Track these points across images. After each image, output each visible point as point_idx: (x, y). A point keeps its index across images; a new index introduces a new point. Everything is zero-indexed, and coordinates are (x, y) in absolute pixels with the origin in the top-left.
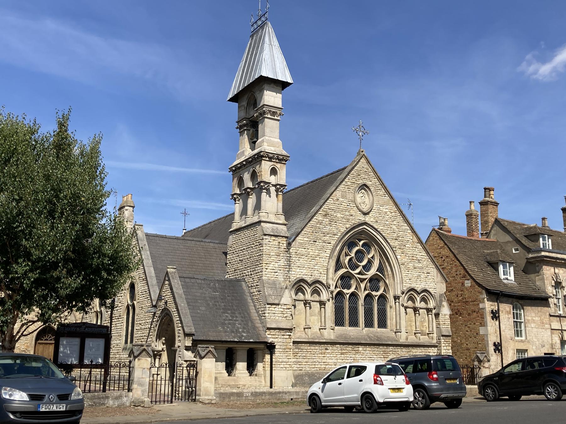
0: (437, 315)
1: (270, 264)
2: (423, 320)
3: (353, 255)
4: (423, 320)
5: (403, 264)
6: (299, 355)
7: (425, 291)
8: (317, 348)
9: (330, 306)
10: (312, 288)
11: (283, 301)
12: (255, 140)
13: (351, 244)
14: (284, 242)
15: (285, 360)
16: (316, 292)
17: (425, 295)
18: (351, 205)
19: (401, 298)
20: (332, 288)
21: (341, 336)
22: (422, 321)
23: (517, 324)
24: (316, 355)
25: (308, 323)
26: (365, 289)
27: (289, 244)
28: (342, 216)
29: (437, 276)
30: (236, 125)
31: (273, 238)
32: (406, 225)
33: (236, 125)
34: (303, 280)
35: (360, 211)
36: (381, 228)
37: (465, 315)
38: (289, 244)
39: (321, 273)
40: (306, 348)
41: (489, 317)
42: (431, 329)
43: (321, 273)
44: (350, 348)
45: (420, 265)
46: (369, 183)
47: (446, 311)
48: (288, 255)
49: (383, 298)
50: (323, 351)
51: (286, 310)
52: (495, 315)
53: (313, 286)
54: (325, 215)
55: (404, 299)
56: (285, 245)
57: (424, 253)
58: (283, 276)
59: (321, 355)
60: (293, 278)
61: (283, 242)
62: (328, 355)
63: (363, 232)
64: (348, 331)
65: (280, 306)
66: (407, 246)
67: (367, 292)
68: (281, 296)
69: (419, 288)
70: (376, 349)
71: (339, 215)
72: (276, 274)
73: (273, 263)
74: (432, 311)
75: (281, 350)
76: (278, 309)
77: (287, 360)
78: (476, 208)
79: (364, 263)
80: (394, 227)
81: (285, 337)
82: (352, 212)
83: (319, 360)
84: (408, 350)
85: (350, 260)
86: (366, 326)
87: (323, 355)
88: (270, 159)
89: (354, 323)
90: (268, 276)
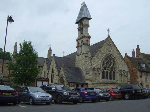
0: (127, 76)
3: (107, 62)
7: (124, 70)
9: (101, 74)
12: (82, 33)
13: (106, 59)
16: (98, 71)
20: (102, 70)
23: (146, 79)
25: (96, 78)
26: (110, 70)
27: (91, 59)
30: (77, 29)
31: (87, 57)
33: (77, 29)
34: (95, 68)
35: (109, 50)
37: (133, 76)
38: (91, 59)
41: (139, 77)
44: (106, 84)
45: (123, 64)
46: (111, 44)
47: (129, 75)
49: (114, 73)
52: (141, 77)
55: (119, 73)
57: (124, 61)
64: (106, 80)
67: (110, 71)
68: (89, 72)
76: (89, 75)
78: (135, 50)
79: (109, 64)
85: (106, 63)
89: (107, 78)
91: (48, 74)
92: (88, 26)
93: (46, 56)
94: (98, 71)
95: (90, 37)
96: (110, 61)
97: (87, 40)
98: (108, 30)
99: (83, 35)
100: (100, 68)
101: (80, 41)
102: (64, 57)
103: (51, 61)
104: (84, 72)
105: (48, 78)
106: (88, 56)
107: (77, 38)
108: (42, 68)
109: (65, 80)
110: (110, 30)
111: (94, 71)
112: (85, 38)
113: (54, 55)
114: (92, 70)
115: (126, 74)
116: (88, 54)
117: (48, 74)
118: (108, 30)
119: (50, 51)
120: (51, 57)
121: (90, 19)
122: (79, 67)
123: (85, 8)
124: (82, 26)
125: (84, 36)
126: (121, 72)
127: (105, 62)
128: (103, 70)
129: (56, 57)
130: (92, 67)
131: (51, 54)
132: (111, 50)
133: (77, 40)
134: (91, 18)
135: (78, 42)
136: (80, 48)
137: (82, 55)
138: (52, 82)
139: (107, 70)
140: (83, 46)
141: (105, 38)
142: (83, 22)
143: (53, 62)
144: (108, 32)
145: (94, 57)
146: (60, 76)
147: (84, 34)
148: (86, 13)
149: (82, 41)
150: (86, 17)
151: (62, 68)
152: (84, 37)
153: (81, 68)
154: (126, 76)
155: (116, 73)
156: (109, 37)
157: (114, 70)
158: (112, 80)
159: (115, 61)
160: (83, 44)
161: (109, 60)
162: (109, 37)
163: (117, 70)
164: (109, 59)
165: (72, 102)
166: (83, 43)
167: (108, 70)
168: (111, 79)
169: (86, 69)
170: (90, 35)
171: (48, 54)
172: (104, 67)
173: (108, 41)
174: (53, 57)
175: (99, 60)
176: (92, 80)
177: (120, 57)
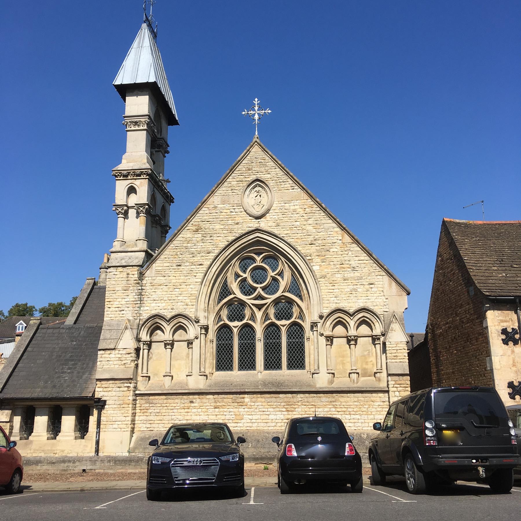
1: (114, 301)
2: (366, 353)
4: (366, 353)
5: (324, 277)
6: (150, 411)
8: (176, 401)
10: (172, 324)
11: (121, 345)
14: (134, 273)
15: (119, 419)
17: (366, 316)
18: (236, 210)
19: (319, 325)
21: (216, 384)
22: (364, 356)
24: (174, 411)
27: (141, 275)
28: (222, 227)
29: (390, 285)
31: (120, 269)
32: (330, 221)
36: (286, 232)
38: (141, 275)
39: (187, 305)
40: (160, 402)
42: (379, 367)
43: (187, 305)
48: (140, 288)
49: (296, 330)
50: (186, 405)
51: (125, 356)
53: (175, 321)
54: (197, 230)
56: (136, 276)
58: (132, 313)
60: (145, 316)
61: (133, 273)
62: (193, 410)
63: (258, 242)
64: (236, 376)
65: (117, 352)
66: (331, 250)
69: (351, 307)
70: (274, 399)
71: (218, 227)
72: (122, 312)
73: (118, 300)
74: (379, 339)
75: (115, 406)
76: (114, 355)
77: (124, 419)
80: (310, 228)
81: (121, 389)
82: (239, 219)
83: (179, 417)
84: (330, 400)
86: (239, 370)
87: (186, 410)
88: (126, 176)
89: (247, 363)
90: (110, 316)
128: (269, 279)
158: (285, 374)
165: (87, 422)
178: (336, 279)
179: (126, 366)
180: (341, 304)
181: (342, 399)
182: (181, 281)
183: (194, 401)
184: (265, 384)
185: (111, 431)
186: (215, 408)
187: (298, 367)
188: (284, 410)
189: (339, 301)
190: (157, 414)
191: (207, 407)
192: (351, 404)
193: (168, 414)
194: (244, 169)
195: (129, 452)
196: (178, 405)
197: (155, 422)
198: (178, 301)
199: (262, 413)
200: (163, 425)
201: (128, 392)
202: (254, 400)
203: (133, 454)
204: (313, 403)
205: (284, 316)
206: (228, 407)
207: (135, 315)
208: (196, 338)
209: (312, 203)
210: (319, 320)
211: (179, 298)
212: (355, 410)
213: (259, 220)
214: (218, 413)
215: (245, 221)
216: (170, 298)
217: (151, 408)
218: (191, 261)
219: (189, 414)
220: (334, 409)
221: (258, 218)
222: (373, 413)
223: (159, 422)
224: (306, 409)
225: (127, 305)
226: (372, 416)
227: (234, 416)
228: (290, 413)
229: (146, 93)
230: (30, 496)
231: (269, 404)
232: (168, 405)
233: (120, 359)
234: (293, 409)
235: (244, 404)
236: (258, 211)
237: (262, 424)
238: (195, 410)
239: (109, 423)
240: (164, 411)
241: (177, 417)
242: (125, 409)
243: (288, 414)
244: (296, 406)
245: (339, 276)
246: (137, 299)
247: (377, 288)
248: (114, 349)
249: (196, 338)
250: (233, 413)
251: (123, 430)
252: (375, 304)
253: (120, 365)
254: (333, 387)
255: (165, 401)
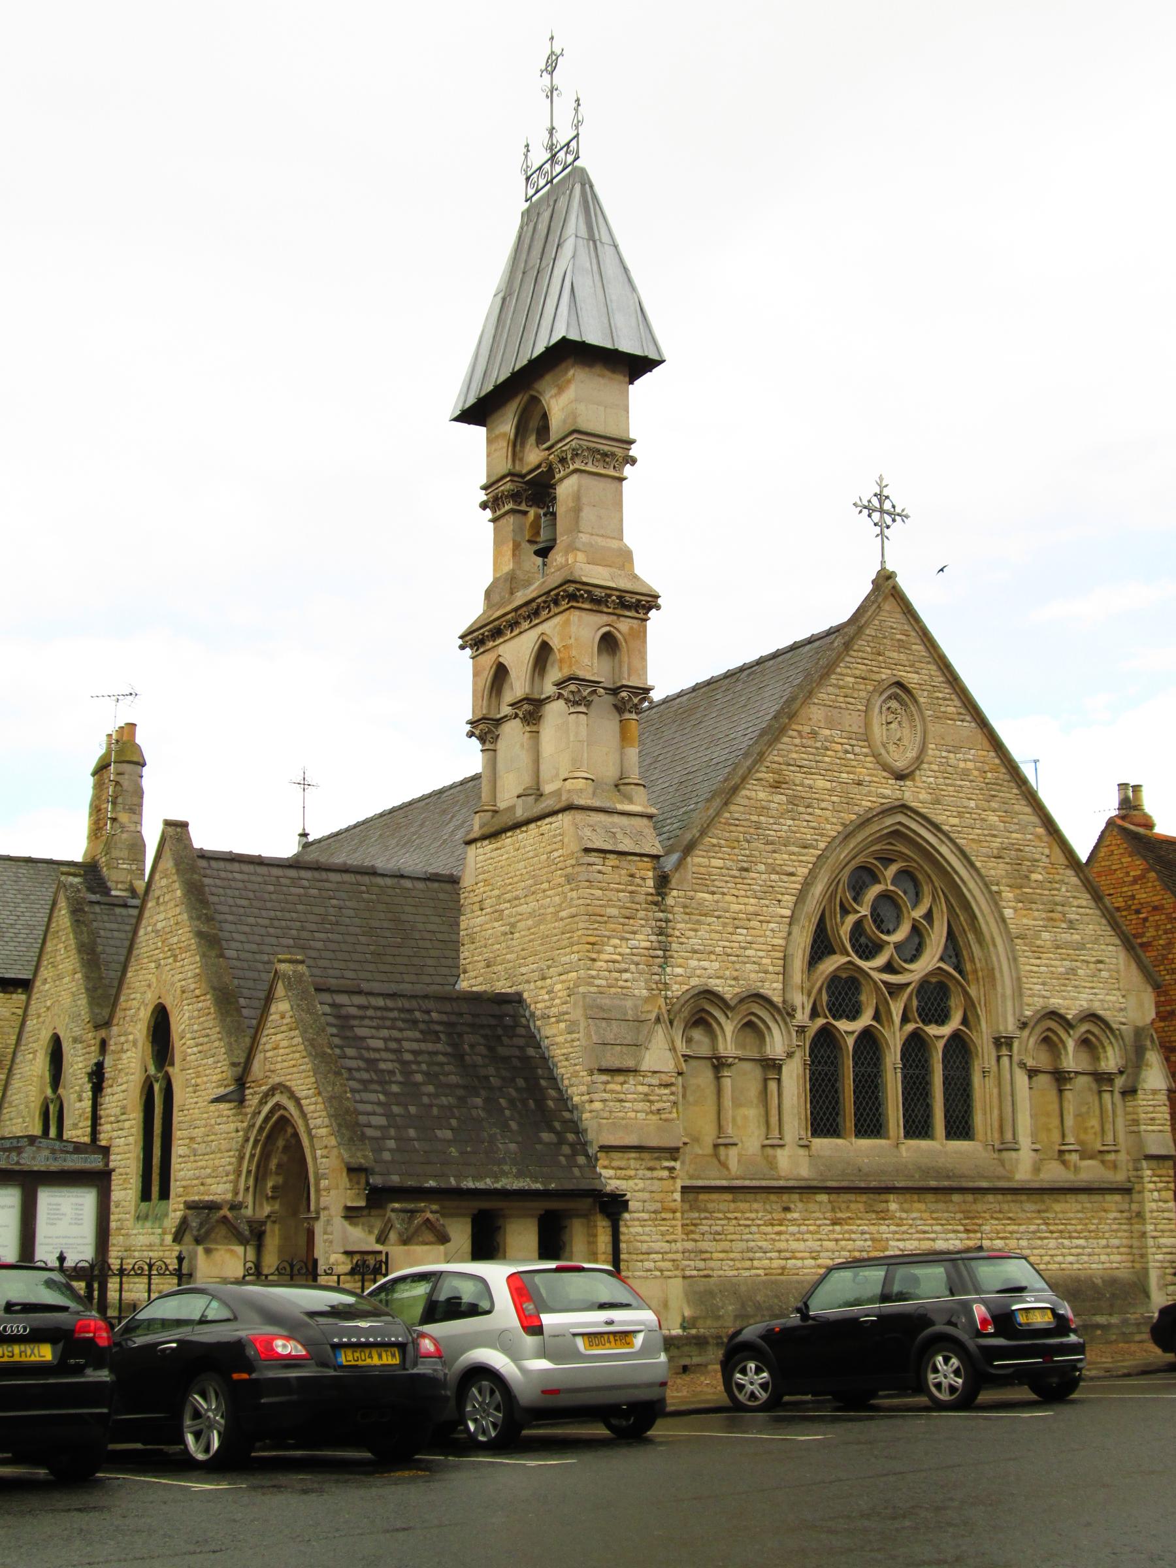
0: (1130, 1092)
2: (1084, 1109)
3: (865, 911)
4: (1084, 1109)
7: (1092, 1017)
8: (755, 1206)
9: (794, 1077)
13: (863, 876)
18: (857, 750)
20: (802, 1017)
26: (905, 1019)
27: (663, 882)
30: (482, 496)
31: (612, 860)
34: (709, 994)
35: (885, 767)
38: (663, 882)
43: (766, 972)
44: (858, 1204)
46: (912, 679)
47: (1155, 1078)
49: (959, 1047)
55: (1028, 1048)
56: (650, 883)
59: (769, 1229)
64: (852, 1151)
67: (910, 1027)
71: (821, 783)
76: (632, 1087)
77: (666, 1247)
79: (875, 890)
82: (862, 773)
91: (97, 1078)
92: (612, 454)
93: (72, 845)
94: (751, 1028)
95: (641, 603)
96: (905, 899)
97: (609, 643)
98: (881, 511)
99: (554, 579)
100: (772, 989)
101: (517, 651)
102: (306, 846)
103: (137, 903)
104: (566, 1046)
105: (94, 1133)
106: (626, 845)
107: (471, 610)
108: (19, 997)
109: (326, 1156)
110: (898, 498)
111: (697, 1034)
112: (574, 616)
113: (176, 830)
114: (679, 1025)
115: (1111, 1061)
116: (624, 820)
117: (97, 1078)
118: (881, 511)
119: (119, 770)
120: (138, 846)
121: (637, 366)
122: (502, 987)
123: (575, 224)
124: (533, 456)
125: (571, 588)
126: (1049, 1043)
127: (845, 911)
129: (203, 855)
130: (677, 990)
131: (136, 809)
132: (919, 760)
133: (478, 639)
134: (653, 355)
135: (488, 660)
136: (513, 733)
137: (544, 825)
138: (156, 1180)
139: (865, 1020)
140: (555, 711)
141: (837, 604)
142: (547, 406)
143: (167, 923)
144: (882, 527)
145: (697, 860)
146: (262, 1102)
147: (576, 561)
148: (586, 288)
149: (544, 652)
150: (595, 337)
151: (281, 1007)
152: (573, 595)
153: (537, 998)
154: (1119, 1082)
155: (985, 1054)
156: (885, 587)
157: (965, 1021)
158: (939, 1150)
159: (967, 907)
160: (549, 689)
161: (892, 878)
162: (885, 587)
163: (1002, 1014)
164: (893, 869)
166: (554, 674)
167: (877, 1017)
168: (918, 1127)
169: (598, 1014)
170: (649, 570)
171: (96, 809)
172: (834, 981)
173: (881, 652)
174: (168, 864)
175: (769, 890)
176: (673, 1152)
177: (1041, 849)
178: (1042, 943)
179: (663, 1116)
180: (1052, 1001)
181: (1057, 1207)
182: (751, 909)
183: (792, 1206)
184: (926, 1172)
185: (640, 1277)
186: (834, 1224)
187: (872, 1132)
188: (961, 1228)
189: (1047, 994)
190: (718, 1237)
191: (818, 1222)
192: (1072, 1215)
193: (738, 1237)
194: (869, 649)
195: (684, 1328)
196: (760, 1215)
197: (715, 1255)
198: (746, 960)
199: (922, 1236)
200: (731, 1263)
201: (671, 1181)
202: (906, 1206)
203: (693, 1331)
204: (1010, 1215)
205: (933, 1015)
206: (859, 1222)
207: (654, 986)
208: (1121, 1072)
209: (997, 761)
210: (1018, 1033)
211: (748, 952)
212: (1079, 1227)
213: (902, 783)
214: (840, 1236)
215: (875, 779)
216: (729, 951)
217: (704, 1222)
218: (770, 861)
219: (783, 1237)
220: (1043, 1227)
221: (900, 777)
222: (1107, 1235)
223: (722, 1255)
224: (999, 1227)
225: (636, 958)
226: (1104, 1242)
227: (869, 1243)
228: (972, 1235)
229: (564, 365)
230: (668, 1430)
231: (935, 1215)
232: (739, 1215)
233: (646, 1098)
234: (976, 1228)
235: (890, 1214)
236: (900, 759)
237: (1071, 1259)
238: (792, 1229)
239: (635, 1257)
240: (731, 1229)
241: (760, 1244)
242: (668, 1223)
243: (969, 1239)
244: (980, 1221)
245: (1046, 935)
246: (656, 945)
247: (509, 901)
248: (635, 1071)
249: (1121, 1072)
250: (867, 1236)
251: (666, 1273)
252: (1106, 1006)
253: (647, 1114)
254: (1042, 1181)
255: (732, 1205)
